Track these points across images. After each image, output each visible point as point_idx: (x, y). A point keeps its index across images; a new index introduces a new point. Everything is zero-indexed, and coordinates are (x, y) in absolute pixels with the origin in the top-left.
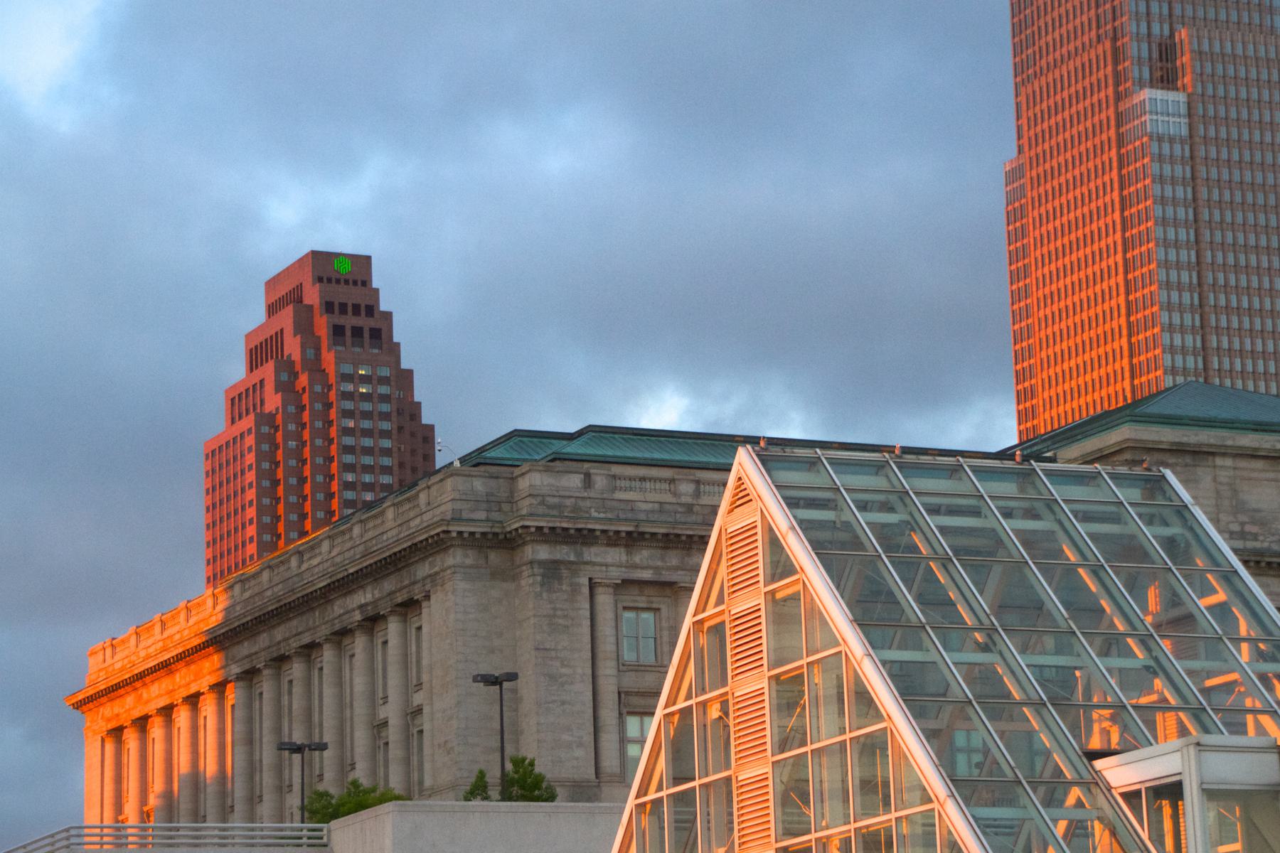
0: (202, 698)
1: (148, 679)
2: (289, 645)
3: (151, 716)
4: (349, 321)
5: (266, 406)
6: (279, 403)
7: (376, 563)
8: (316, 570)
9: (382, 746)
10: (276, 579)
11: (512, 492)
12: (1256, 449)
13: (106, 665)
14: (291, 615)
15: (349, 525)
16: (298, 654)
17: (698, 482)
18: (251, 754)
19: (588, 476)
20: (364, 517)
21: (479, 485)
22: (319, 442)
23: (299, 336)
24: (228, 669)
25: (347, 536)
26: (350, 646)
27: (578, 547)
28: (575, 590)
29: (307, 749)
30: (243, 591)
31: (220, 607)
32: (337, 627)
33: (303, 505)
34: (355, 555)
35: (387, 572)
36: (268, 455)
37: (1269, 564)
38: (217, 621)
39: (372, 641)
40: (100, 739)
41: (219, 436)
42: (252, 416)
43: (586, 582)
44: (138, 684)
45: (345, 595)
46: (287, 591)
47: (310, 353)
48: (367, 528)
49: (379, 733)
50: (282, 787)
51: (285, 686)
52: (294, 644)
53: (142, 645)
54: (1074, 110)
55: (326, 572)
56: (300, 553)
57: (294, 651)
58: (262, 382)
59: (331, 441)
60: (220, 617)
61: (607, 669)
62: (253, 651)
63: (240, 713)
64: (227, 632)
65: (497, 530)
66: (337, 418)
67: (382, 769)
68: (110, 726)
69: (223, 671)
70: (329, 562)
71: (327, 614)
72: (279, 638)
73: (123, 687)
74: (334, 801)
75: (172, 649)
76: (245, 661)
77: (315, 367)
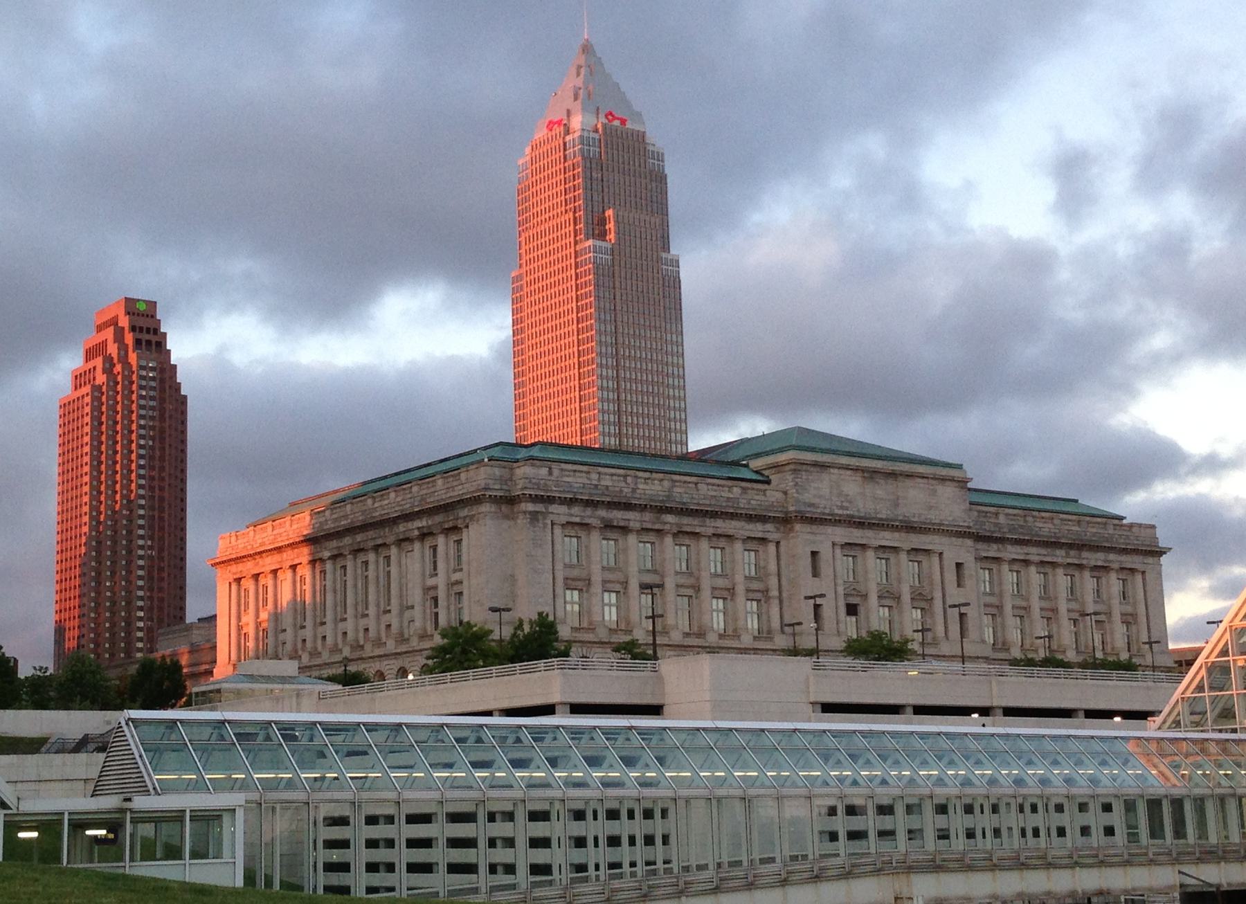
4: (145, 337)
6: (105, 380)
11: (512, 475)
12: (849, 465)
16: (372, 549)
17: (599, 473)
19: (550, 468)
21: (497, 471)
27: (546, 504)
28: (545, 525)
30: (331, 514)
36: (97, 409)
37: (854, 522)
43: (550, 522)
47: (122, 353)
52: (371, 544)
53: (257, 537)
54: (551, 247)
61: (559, 566)
65: (507, 495)
77: (124, 360)
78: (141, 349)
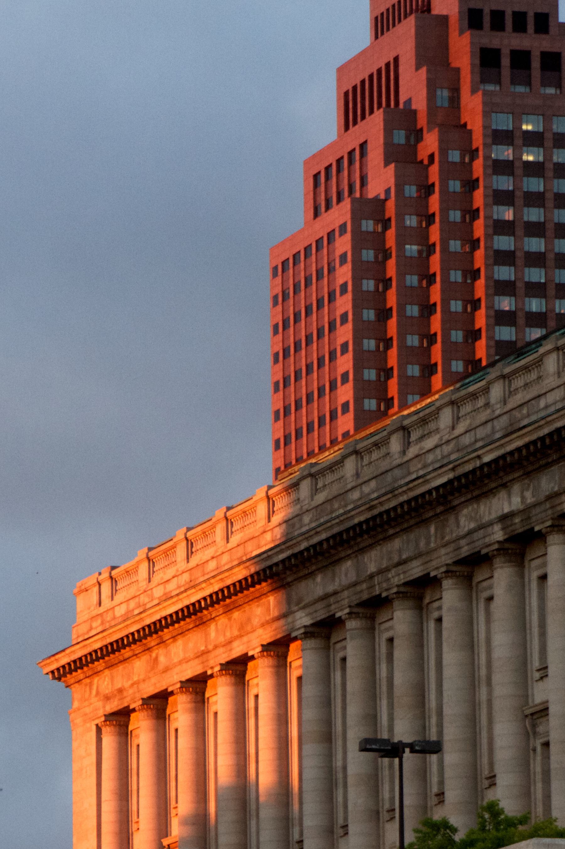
0: (251, 664)
1: (166, 634)
2: (388, 580)
3: (172, 693)
5: (369, 186)
6: (392, 182)
7: (527, 446)
8: (430, 458)
9: (539, 749)
10: (367, 473)
13: (101, 610)
14: (391, 532)
15: (483, 383)
18: (329, 756)
20: (507, 370)
22: (455, 245)
23: (424, 70)
24: (290, 619)
25: (481, 402)
26: (485, 584)
29: (407, 750)
30: (315, 491)
31: (277, 518)
32: (465, 551)
33: (427, 352)
34: (493, 432)
35: (542, 462)
38: (273, 541)
39: (522, 576)
40: (94, 728)
41: (293, 236)
42: (347, 204)
44: (152, 641)
45: (477, 499)
46: (383, 491)
47: (443, 94)
48: (513, 387)
49: (534, 726)
50: (378, 812)
51: (383, 648)
53: (156, 579)
55: (445, 461)
56: (405, 430)
57: (395, 590)
58: (363, 146)
59: (475, 244)
60: (278, 533)
62: (330, 588)
63: (309, 690)
64: (289, 558)
66: (486, 205)
67: (539, 785)
68: (113, 706)
69: (282, 622)
70: (452, 445)
71: (448, 530)
72: (372, 568)
73: (129, 645)
74: (457, 838)
75: (204, 585)
76: (319, 606)
78: (499, 82)
